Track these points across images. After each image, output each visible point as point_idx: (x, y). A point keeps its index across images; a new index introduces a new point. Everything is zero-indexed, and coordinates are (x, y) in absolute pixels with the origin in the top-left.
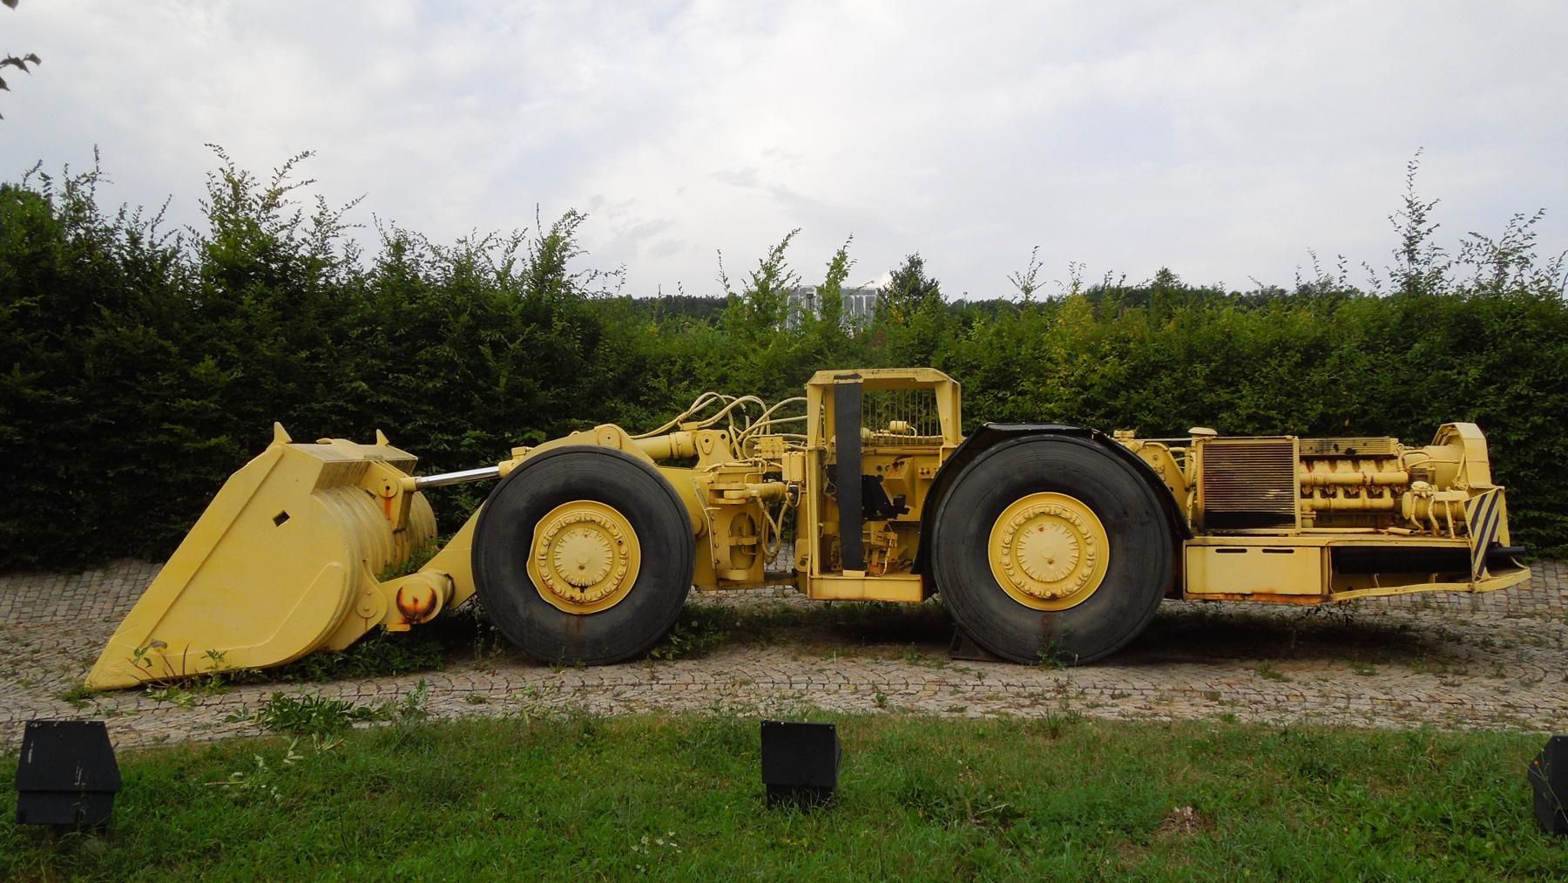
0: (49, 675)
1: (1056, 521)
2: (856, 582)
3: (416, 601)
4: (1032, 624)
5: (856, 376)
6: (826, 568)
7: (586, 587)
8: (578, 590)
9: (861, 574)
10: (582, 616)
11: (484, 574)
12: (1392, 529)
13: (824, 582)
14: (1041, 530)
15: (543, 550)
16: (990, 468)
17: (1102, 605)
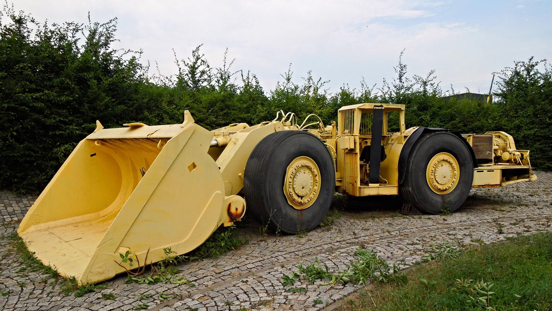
0: (316, 263)
1: (446, 162)
2: (376, 188)
3: (237, 209)
4: (439, 199)
5: (382, 106)
6: (362, 182)
7: (303, 197)
8: (300, 198)
9: (378, 185)
10: (302, 210)
11: (268, 193)
12: (499, 163)
13: (365, 189)
14: (442, 166)
15: (291, 180)
16: (429, 142)
17: (458, 192)
